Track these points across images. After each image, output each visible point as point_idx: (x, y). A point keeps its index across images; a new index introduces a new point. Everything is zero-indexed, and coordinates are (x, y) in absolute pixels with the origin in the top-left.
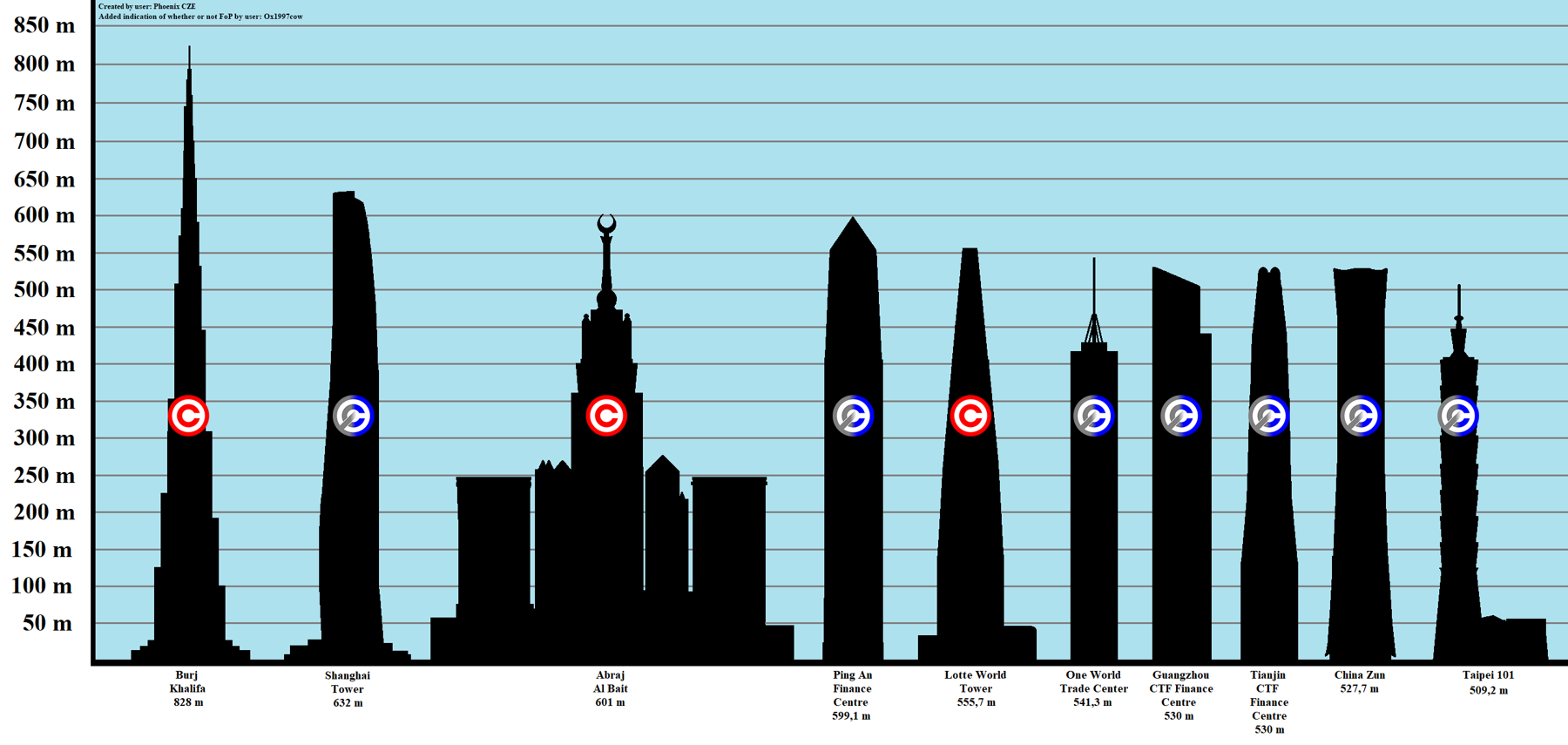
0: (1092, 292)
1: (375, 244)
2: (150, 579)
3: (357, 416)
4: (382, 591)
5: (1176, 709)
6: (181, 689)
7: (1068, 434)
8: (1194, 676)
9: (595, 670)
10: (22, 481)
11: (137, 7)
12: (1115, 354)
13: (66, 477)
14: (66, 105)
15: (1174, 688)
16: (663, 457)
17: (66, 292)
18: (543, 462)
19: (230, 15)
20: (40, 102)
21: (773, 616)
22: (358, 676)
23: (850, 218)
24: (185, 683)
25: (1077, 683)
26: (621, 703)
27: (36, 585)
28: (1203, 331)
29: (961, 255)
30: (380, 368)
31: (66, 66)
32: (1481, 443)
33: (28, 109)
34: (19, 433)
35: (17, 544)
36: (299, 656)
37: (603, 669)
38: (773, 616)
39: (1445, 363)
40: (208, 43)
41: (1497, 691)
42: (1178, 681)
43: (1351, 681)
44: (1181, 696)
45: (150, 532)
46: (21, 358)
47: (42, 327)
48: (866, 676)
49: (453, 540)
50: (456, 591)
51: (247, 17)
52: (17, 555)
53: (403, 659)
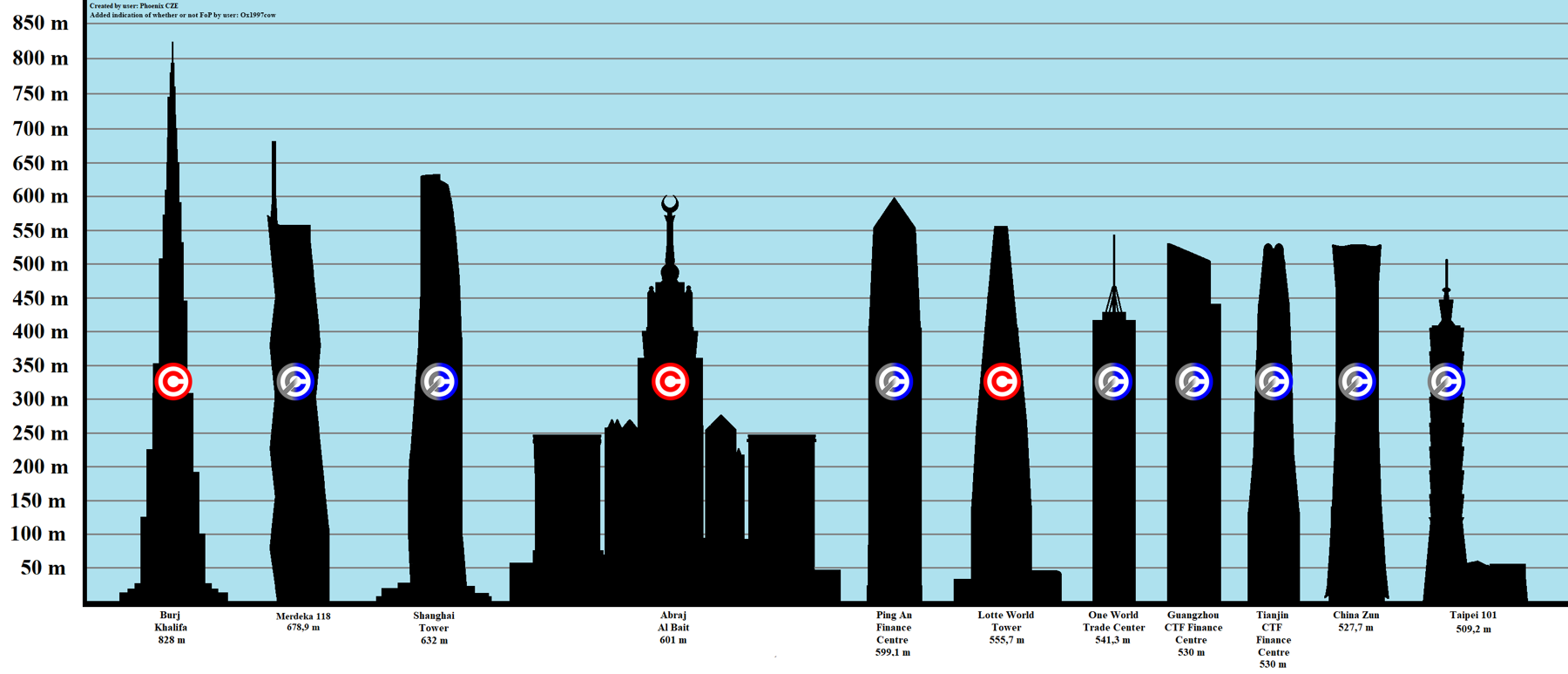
0: (1112, 266)
1: (459, 223)
2: (137, 528)
3: (443, 382)
4: (465, 538)
5: (1189, 646)
6: (165, 628)
7: (977, 395)
8: (1205, 616)
9: (660, 610)
10: (20, 439)
11: (125, 7)
12: (1133, 322)
13: (60, 435)
14: (60, 96)
15: (1186, 627)
16: (721, 417)
17: (60, 266)
18: (612, 421)
19: (210, 14)
20: (36, 93)
21: (822, 561)
22: (444, 616)
23: (891, 199)
24: (169, 622)
25: (1098, 622)
26: (683, 641)
27: (33, 533)
28: (1213, 302)
29: (993, 233)
30: (464, 335)
31: (60, 60)
32: (1466, 403)
33: (26, 99)
34: (17, 395)
35: (15, 495)
36: (390, 598)
37: (666, 609)
38: (822, 561)
39: (1433, 330)
40: (190, 39)
41: (1481, 630)
42: (1190, 621)
43: (1349, 621)
44: (1193, 634)
45: (136, 485)
46: (20, 327)
47: (38, 298)
48: (906, 616)
49: (530, 491)
50: (866, 538)
51: (225, 16)
52: (15, 506)
53: (484, 600)
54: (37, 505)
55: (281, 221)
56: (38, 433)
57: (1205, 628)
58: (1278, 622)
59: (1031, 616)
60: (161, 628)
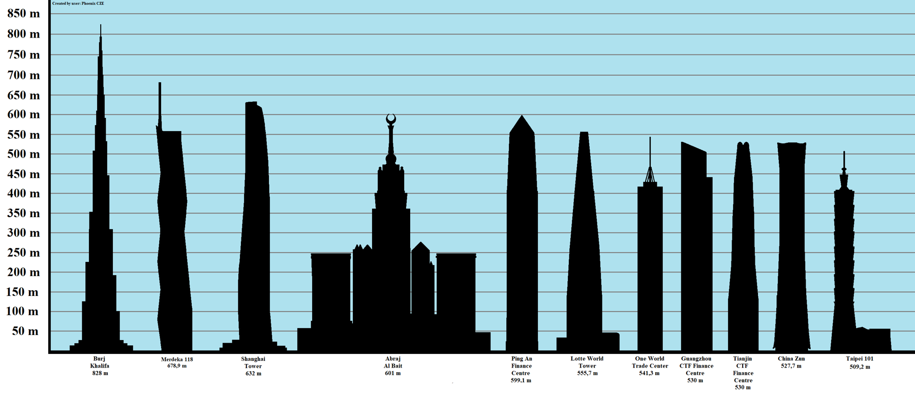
0: (649, 155)
1: (268, 130)
2: (80, 308)
4: (271, 314)
5: (694, 377)
6: (96, 366)
8: (703, 359)
9: (385, 356)
10: (12, 256)
12: (661, 188)
13: (35, 254)
14: (35, 56)
15: (692, 366)
16: (421, 243)
17: (35, 155)
18: (357, 245)
20: (21, 54)
21: (480, 327)
22: (259, 359)
23: (520, 116)
24: (99, 363)
25: (641, 363)
26: (398, 374)
27: (19, 311)
28: (708, 176)
29: (579, 136)
30: (271, 196)
31: (35, 35)
33: (15, 58)
34: (10, 230)
35: (9, 289)
36: (227, 349)
37: (389, 355)
38: (480, 327)
39: (836, 193)
41: (865, 367)
42: (695, 362)
43: (787, 362)
44: (696, 370)
45: (79, 283)
46: (11, 190)
47: (22, 174)
48: (529, 359)
49: (309, 287)
50: (506, 314)
52: (9, 295)
53: (283, 350)
54: (21, 294)
55: (164, 129)
56: (22, 252)
57: (703, 366)
58: (746, 363)
59: (602, 359)
60: (94, 366)
